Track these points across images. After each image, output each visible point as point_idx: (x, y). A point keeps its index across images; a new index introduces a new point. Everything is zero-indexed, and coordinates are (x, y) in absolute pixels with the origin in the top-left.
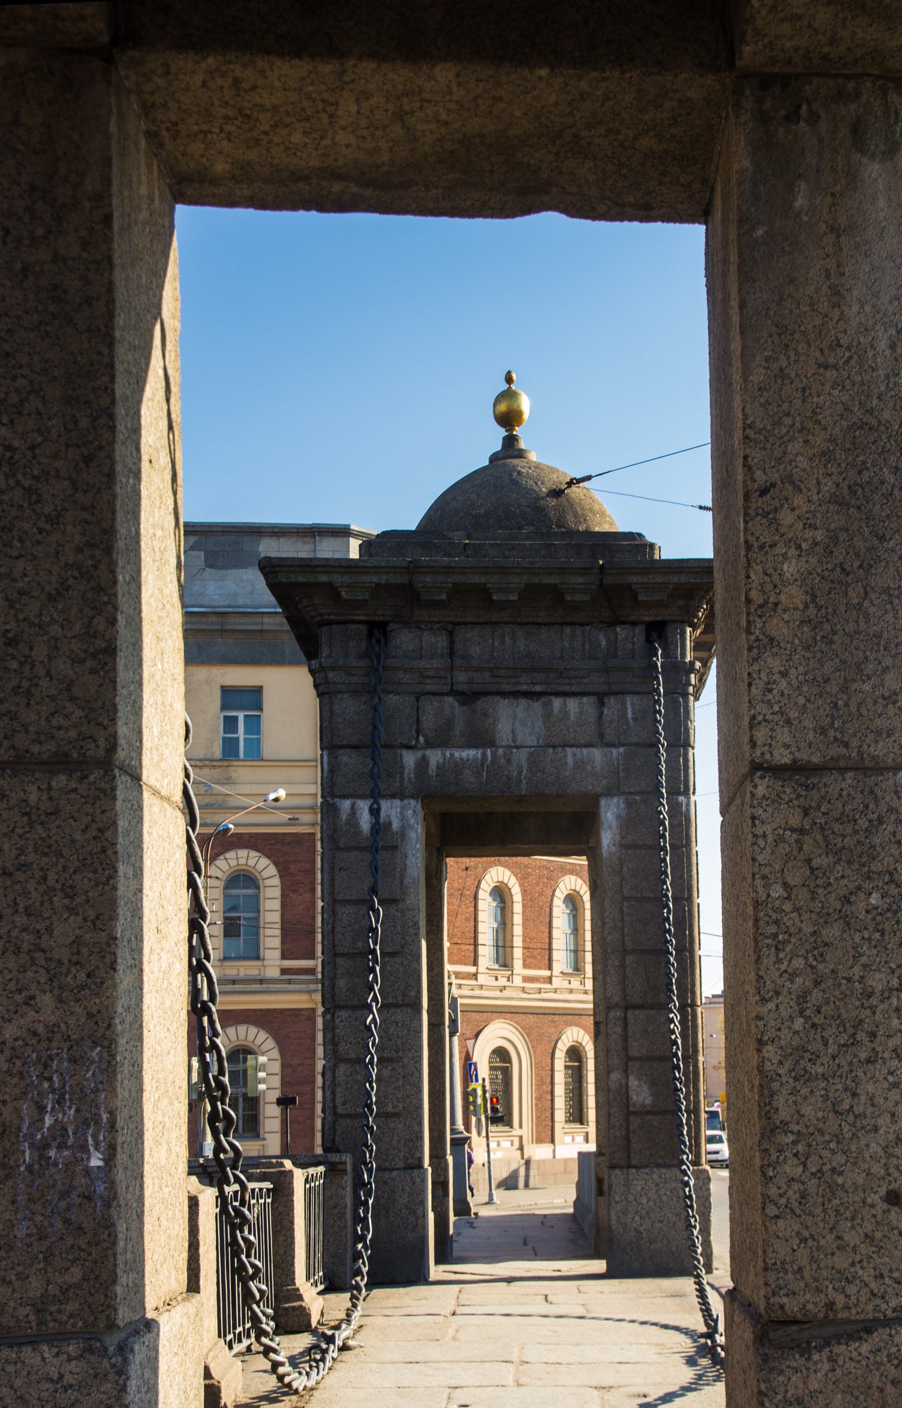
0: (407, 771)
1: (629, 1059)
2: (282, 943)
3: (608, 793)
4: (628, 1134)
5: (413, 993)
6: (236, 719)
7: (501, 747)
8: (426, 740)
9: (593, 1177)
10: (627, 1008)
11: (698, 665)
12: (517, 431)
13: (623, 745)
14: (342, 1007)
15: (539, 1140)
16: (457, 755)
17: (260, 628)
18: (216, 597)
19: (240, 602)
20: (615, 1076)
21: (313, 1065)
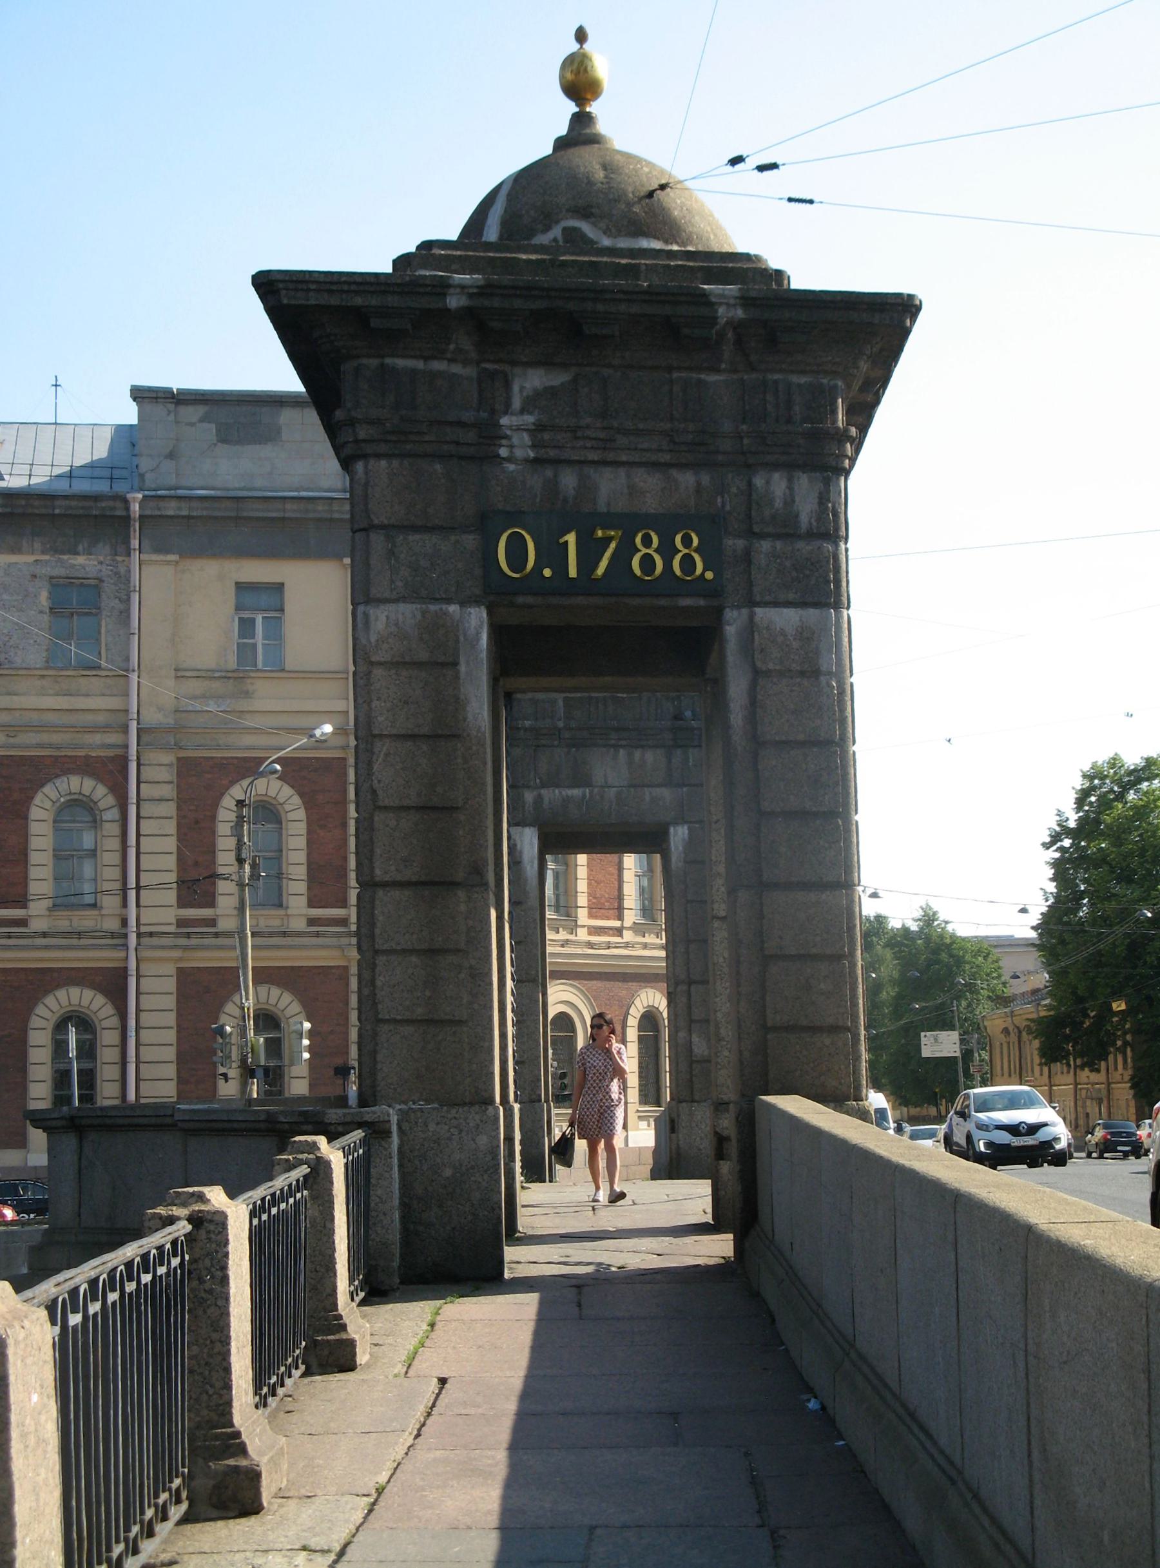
0: (527, 805)
1: (692, 1021)
2: (309, 888)
3: (680, 820)
4: (691, 1078)
5: (533, 972)
6: (253, 621)
7: (597, 787)
8: (541, 782)
9: (668, 1118)
11: (853, 431)
12: (593, 108)
13: (686, 786)
16: (564, 793)
19: (259, 483)
20: (682, 1034)
21: (346, 1034)
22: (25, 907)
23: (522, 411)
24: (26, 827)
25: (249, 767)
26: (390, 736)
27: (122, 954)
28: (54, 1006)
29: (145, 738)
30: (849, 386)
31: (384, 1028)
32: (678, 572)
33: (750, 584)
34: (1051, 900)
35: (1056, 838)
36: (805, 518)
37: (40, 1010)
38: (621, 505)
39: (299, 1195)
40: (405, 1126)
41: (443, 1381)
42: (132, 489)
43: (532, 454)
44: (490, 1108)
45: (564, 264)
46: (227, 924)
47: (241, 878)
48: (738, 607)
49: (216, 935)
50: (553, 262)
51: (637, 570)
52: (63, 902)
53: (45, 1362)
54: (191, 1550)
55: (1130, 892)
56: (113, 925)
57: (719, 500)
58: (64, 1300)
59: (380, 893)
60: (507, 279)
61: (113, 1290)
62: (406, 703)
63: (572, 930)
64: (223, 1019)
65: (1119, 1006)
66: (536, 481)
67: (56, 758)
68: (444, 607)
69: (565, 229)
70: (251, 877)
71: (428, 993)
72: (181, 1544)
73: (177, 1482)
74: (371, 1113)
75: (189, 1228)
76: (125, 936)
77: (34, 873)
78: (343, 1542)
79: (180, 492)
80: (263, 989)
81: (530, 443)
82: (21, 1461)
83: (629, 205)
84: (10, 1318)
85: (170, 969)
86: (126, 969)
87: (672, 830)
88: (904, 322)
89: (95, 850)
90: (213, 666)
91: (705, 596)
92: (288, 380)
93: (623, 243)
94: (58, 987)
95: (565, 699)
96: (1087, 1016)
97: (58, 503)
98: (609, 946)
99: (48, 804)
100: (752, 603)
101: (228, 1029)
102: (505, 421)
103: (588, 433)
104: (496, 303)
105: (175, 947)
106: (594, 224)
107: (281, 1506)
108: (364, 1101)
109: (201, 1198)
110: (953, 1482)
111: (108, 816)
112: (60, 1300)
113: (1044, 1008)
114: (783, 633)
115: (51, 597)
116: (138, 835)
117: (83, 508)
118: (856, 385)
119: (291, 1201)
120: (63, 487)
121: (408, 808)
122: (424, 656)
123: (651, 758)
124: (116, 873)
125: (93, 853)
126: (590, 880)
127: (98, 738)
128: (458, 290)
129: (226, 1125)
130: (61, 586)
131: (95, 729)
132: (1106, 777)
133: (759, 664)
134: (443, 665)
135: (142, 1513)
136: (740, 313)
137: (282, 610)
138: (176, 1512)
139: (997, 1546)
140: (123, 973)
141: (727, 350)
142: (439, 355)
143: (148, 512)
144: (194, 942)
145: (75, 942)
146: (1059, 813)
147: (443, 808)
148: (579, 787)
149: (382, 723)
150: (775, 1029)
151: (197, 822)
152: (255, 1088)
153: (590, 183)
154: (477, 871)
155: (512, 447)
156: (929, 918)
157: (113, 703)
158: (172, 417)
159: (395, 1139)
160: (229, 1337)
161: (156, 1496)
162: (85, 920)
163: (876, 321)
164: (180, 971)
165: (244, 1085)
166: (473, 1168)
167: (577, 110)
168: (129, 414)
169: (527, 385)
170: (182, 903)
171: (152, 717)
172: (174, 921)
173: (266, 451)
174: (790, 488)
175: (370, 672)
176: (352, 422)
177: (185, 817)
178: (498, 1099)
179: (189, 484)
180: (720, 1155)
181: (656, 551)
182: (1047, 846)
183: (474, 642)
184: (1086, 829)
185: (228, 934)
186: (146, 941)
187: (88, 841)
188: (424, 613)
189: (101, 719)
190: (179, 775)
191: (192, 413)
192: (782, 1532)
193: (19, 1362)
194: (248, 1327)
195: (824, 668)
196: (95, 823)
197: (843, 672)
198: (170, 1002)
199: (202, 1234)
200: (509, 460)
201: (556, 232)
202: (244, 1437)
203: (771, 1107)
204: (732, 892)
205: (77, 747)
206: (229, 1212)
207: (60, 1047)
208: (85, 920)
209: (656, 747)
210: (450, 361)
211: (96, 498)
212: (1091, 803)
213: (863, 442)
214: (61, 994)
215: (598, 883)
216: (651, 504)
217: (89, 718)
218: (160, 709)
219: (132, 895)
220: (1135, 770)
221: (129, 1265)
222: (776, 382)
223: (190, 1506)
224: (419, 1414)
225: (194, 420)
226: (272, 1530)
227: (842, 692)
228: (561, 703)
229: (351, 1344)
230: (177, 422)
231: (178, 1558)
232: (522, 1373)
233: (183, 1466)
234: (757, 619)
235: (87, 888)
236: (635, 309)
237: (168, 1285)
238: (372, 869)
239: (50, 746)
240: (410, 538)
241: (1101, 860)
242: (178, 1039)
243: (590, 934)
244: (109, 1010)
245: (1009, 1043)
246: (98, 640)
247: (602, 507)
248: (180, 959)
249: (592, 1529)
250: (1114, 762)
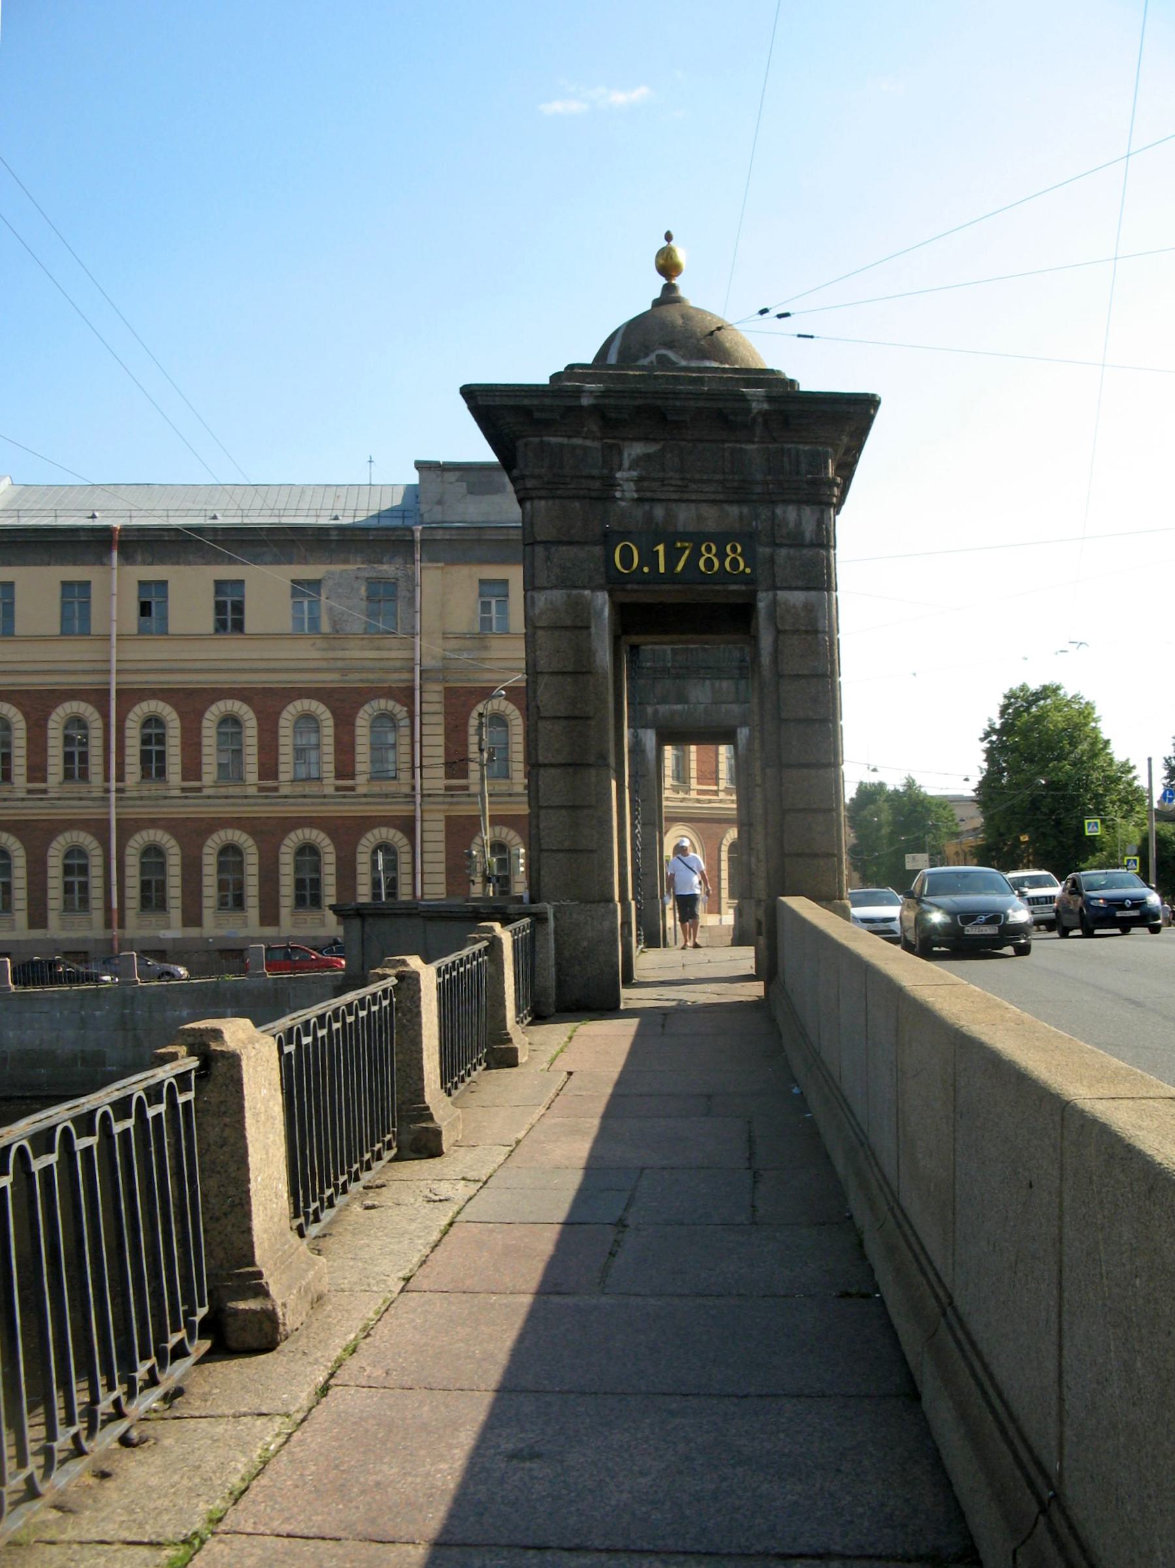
3: (744, 724)
6: (489, 603)
11: (839, 480)
12: (677, 281)
15: (710, 912)
17: (506, 538)
19: (492, 519)
22: (353, 779)
23: (629, 469)
25: (486, 693)
26: (547, 673)
27: (412, 808)
28: (213, 845)
29: (424, 676)
30: (836, 451)
32: (728, 568)
33: (774, 576)
34: (985, 773)
35: (987, 735)
36: (808, 536)
37: (364, 841)
38: (691, 528)
39: (480, 960)
40: (559, 915)
41: (570, 1073)
42: (416, 524)
43: (636, 496)
44: (611, 905)
45: (657, 377)
46: (475, 789)
47: (482, 760)
48: (766, 590)
49: (469, 795)
50: (649, 376)
51: (703, 568)
52: (377, 776)
53: (272, 1069)
54: (395, 1178)
55: (1034, 768)
56: (406, 790)
57: (754, 523)
58: (298, 1029)
59: (542, 771)
60: (619, 387)
61: (337, 1021)
62: (558, 652)
63: (687, 792)
64: (474, 846)
65: (1024, 838)
66: (639, 512)
67: (371, 688)
68: (581, 591)
69: (658, 356)
70: (488, 760)
71: (572, 833)
72: (390, 1174)
73: (389, 1137)
74: (535, 908)
75: (396, 981)
76: (414, 796)
77: (359, 758)
78: (488, 1175)
79: (445, 525)
80: (497, 829)
81: (634, 488)
82: (253, 1130)
83: (698, 340)
84: (246, 1042)
85: (441, 816)
86: (414, 817)
87: (739, 730)
88: (869, 412)
89: (319, 745)
90: (466, 631)
91: (746, 584)
92: (485, 454)
93: (694, 364)
94: (374, 827)
95: (673, 650)
96: (1005, 844)
97: (371, 533)
98: (710, 801)
99: (366, 717)
100: (775, 588)
101: (474, 853)
102: (618, 475)
103: (673, 482)
104: (612, 401)
105: (443, 803)
106: (676, 353)
107: (455, 1151)
108: (533, 900)
109: (404, 963)
110: (862, 1145)
111: (402, 723)
112: (295, 1028)
113: (979, 840)
114: (794, 606)
115: (368, 589)
116: (421, 735)
117: (386, 535)
118: (841, 451)
119: (475, 963)
120: (374, 523)
121: (559, 718)
122: (569, 623)
124: (407, 758)
125: (394, 746)
126: (698, 761)
127: (396, 676)
128: (588, 394)
129: (449, 915)
130: (372, 583)
131: (396, 670)
132: (1018, 697)
133: (780, 627)
134: (581, 628)
135: (362, 1155)
136: (766, 406)
137: (507, 596)
138: (388, 1155)
139: (880, 1186)
140: (413, 818)
141: (759, 430)
142: (577, 434)
143: (425, 538)
144: (455, 800)
145: (383, 800)
146: (990, 720)
147: (582, 718)
148: (680, 703)
149: (543, 664)
151: (456, 727)
152: (491, 889)
153: (674, 327)
154: (603, 757)
155: (623, 491)
156: (910, 784)
157: (405, 654)
158: (439, 479)
159: (552, 923)
160: (421, 1049)
161: (373, 1145)
162: (389, 787)
163: (852, 410)
164: (448, 818)
165: (485, 887)
166: (600, 941)
167: (666, 282)
168: (414, 478)
169: (633, 453)
170: (448, 776)
171: (429, 663)
172: (443, 787)
174: (799, 515)
175: (535, 633)
176: (523, 477)
178: (617, 898)
180: (759, 933)
181: (715, 555)
182: (982, 740)
183: (600, 614)
184: (1006, 729)
185: (474, 795)
186: (426, 799)
187: (391, 739)
188: (569, 596)
189: (398, 664)
190: (445, 697)
191: (451, 477)
192: (762, 1172)
193: (251, 1070)
194: (436, 1042)
195: (820, 629)
196: (395, 727)
197: (833, 631)
198: (441, 836)
199: (404, 985)
200: (621, 499)
201: (652, 357)
202: (432, 1110)
203: (783, 904)
204: (763, 769)
205: (384, 681)
206: (421, 972)
207: (374, 863)
208: (389, 787)
209: (728, 678)
210: (585, 438)
211: (394, 529)
212: (1009, 714)
213: (848, 488)
215: (704, 762)
216: (711, 526)
217: (391, 664)
218: (434, 658)
219: (418, 771)
220: (1036, 693)
221: (349, 1006)
222: (789, 450)
223: (398, 1151)
224: (552, 1095)
226: (447, 1167)
227: (832, 644)
228: (669, 652)
229: (514, 1051)
230: (442, 482)
231: (386, 1183)
232: (619, 1069)
233: (394, 1127)
234: (778, 598)
235: (391, 767)
236: (701, 404)
237: (380, 1018)
238: (537, 756)
239: (367, 681)
240: (560, 548)
241: (1015, 749)
242: (447, 859)
243: (698, 794)
244: (405, 841)
246: (395, 616)
247: (680, 529)
248: (448, 810)
249: (643, 1169)
250: (1023, 688)
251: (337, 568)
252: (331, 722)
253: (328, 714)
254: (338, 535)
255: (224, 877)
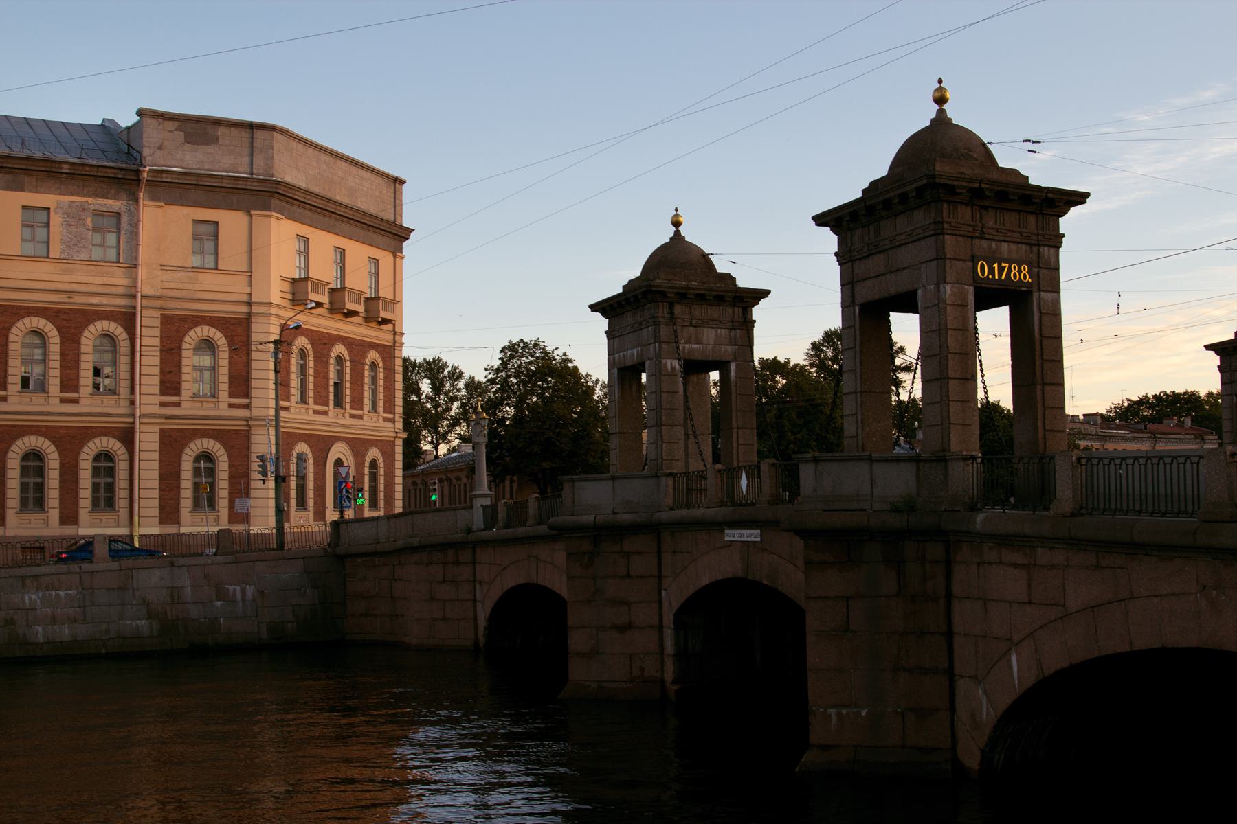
2: (230, 387)
3: (733, 361)
10: (738, 428)
12: (680, 229)
14: (664, 425)
18: (190, 162)
19: (206, 167)
24: (78, 348)
27: (131, 420)
31: (952, 426)
85: (156, 429)
94: (96, 437)
100: (1039, 290)
122: (959, 303)
123: (723, 332)
150: (1048, 431)
164: (162, 430)
167: (939, 108)
170: (163, 393)
173: (210, 149)
177: (164, 346)
179: (169, 164)
191: (171, 125)
198: (156, 446)
214: (97, 441)
216: (1014, 256)
225: (173, 129)
238: (948, 373)
244: (123, 450)
245: (416, 490)
251: (66, 199)
252: (57, 340)
253: (55, 332)
254: (69, 169)
255: (97, 480)
